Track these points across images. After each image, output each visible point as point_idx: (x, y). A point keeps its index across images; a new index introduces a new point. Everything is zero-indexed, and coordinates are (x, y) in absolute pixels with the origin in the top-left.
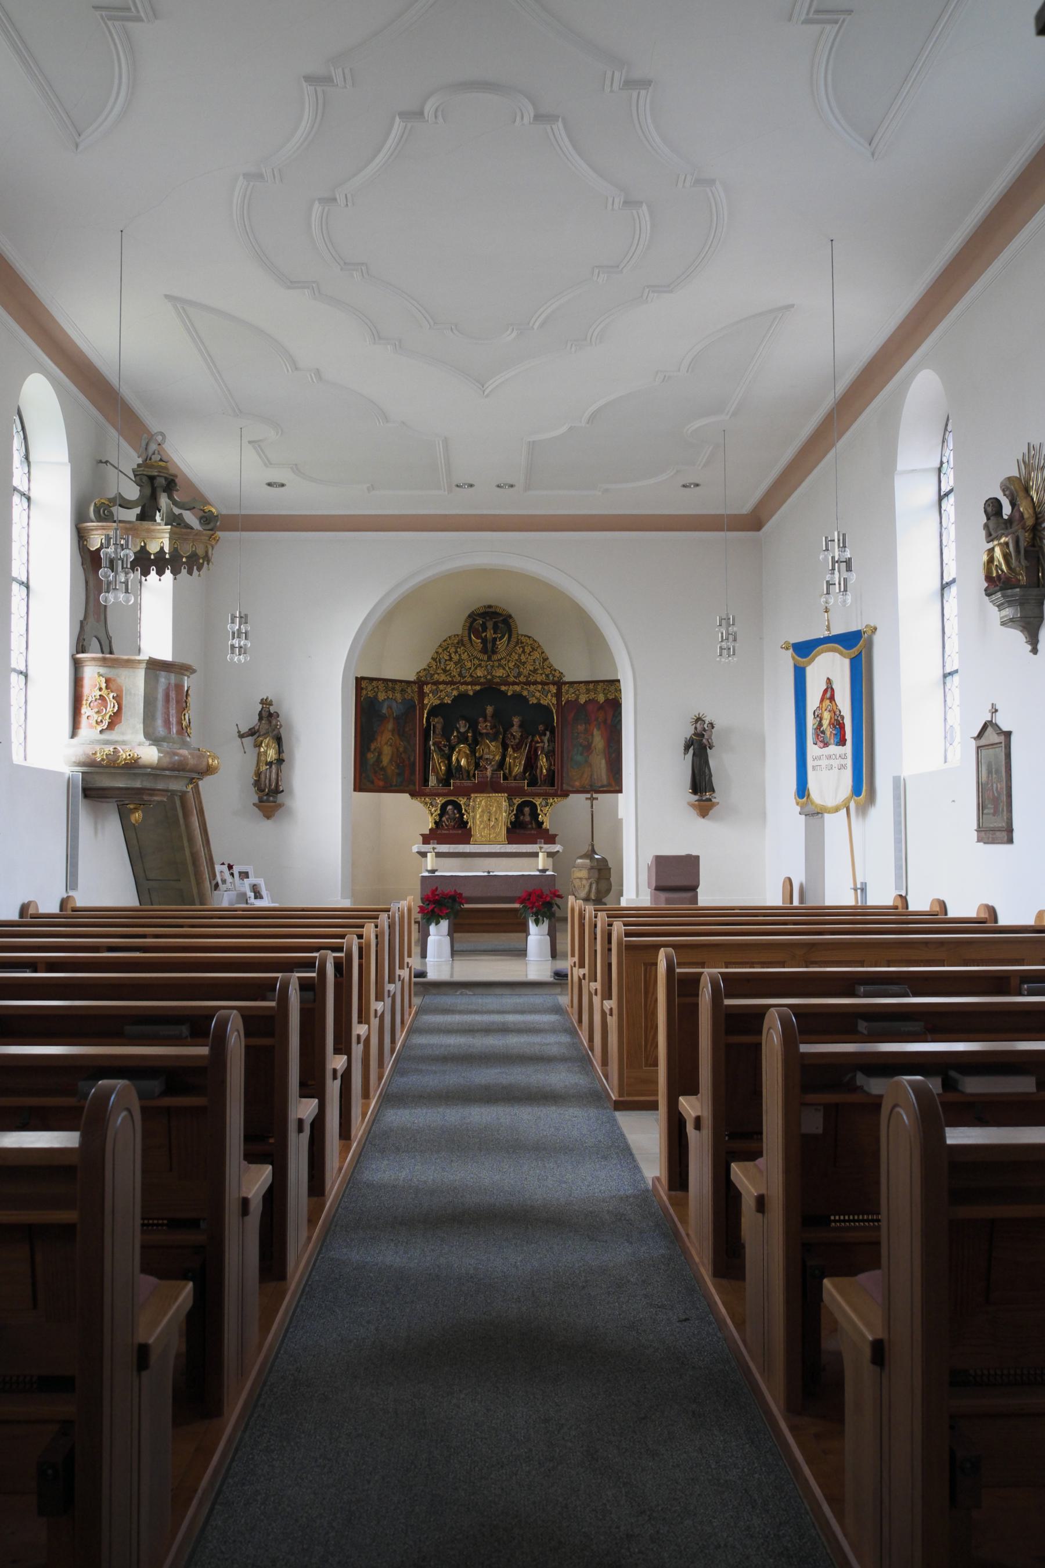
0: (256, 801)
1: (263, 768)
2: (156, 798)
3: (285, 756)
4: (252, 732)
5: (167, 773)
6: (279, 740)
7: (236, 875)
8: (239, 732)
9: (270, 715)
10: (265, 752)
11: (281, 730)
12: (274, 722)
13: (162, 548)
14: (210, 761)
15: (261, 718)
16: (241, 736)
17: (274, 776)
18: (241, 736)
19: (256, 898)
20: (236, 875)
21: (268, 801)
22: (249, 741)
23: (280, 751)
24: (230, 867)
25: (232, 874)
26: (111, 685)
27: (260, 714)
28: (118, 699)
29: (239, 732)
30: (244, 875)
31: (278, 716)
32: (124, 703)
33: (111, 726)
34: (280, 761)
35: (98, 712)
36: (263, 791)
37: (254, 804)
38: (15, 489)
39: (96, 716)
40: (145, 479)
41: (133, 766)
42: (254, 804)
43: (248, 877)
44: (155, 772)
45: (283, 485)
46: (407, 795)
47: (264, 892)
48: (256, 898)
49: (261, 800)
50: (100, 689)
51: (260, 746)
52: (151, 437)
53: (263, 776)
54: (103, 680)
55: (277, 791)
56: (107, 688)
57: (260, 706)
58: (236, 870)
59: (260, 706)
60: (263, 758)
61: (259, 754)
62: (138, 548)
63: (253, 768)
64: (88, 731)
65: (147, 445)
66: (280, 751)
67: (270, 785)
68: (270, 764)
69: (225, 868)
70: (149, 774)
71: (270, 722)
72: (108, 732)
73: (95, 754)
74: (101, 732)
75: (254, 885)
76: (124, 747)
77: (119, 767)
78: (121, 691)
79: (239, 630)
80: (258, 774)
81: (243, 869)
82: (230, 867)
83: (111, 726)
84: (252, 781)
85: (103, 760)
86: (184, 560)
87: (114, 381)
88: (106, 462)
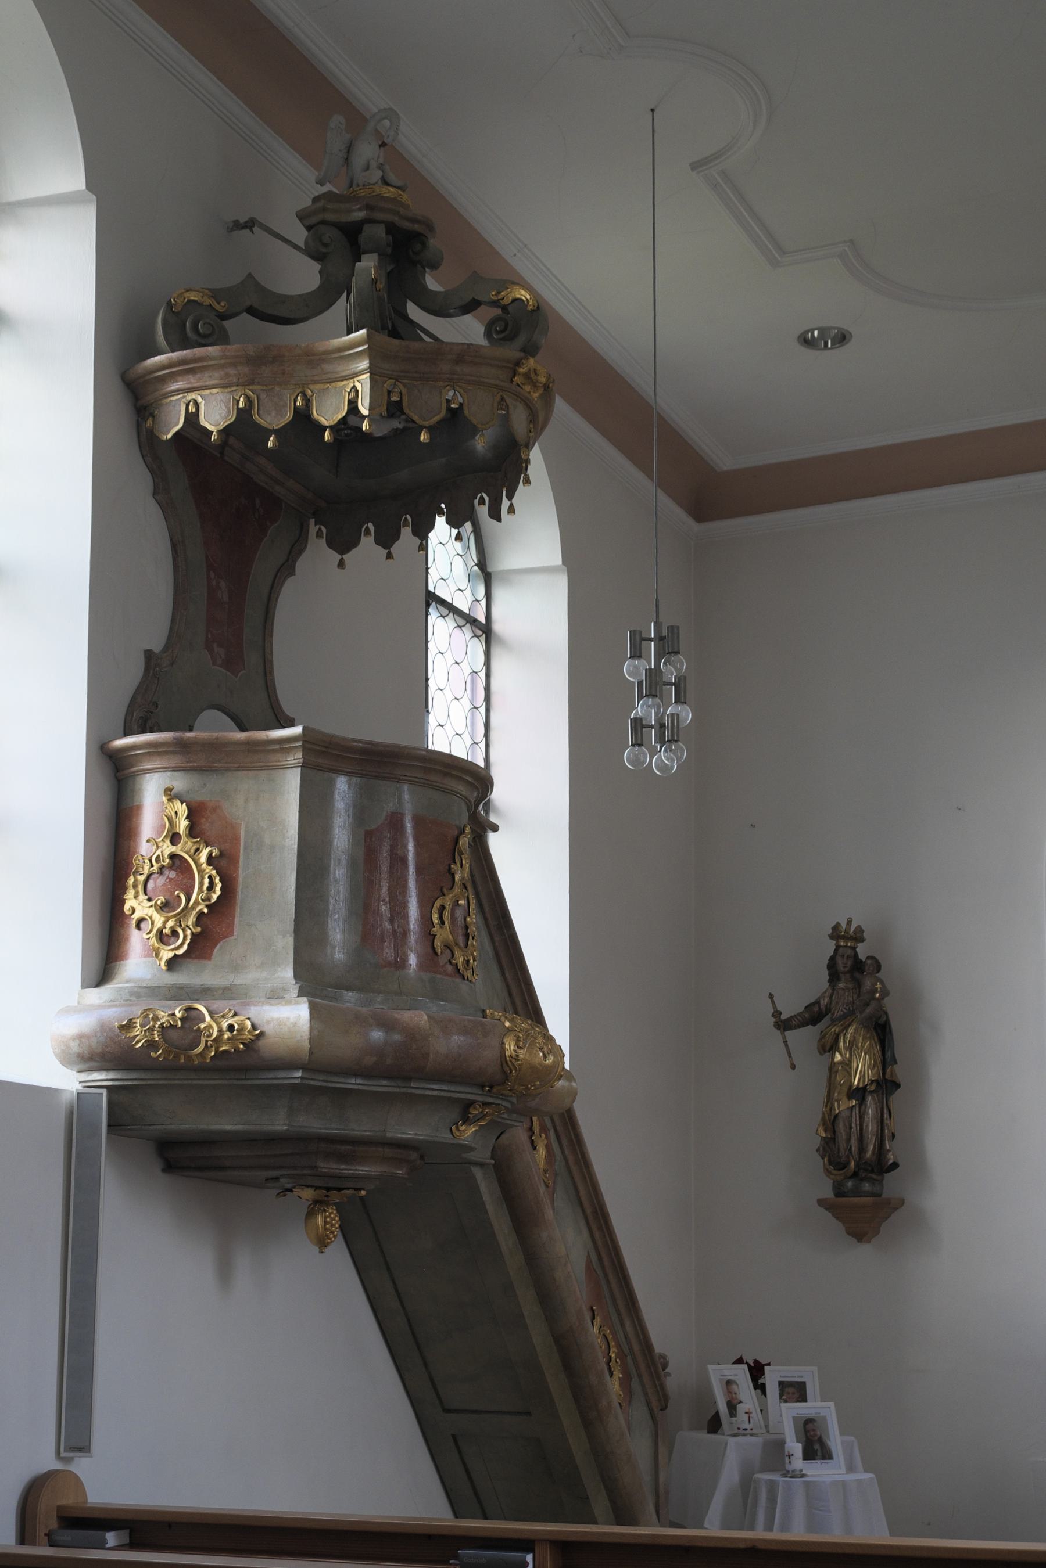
0: (828, 1193)
1: (843, 1105)
2: (364, 1169)
3: (900, 1072)
4: (813, 1015)
5: (353, 1083)
6: (881, 1031)
7: (772, 1389)
8: (777, 1014)
9: (858, 966)
10: (847, 1064)
11: (889, 1003)
12: (867, 983)
13: (353, 405)
14: (510, 1046)
15: (834, 975)
16: (783, 1025)
17: (871, 1126)
18: (783, 1025)
19: (809, 1454)
20: (772, 1389)
21: (857, 1193)
22: (805, 1037)
23: (886, 1058)
24: (757, 1371)
25: (761, 1388)
26: (205, 825)
27: (832, 965)
28: (224, 864)
29: (777, 1014)
30: (794, 1391)
31: (878, 967)
32: (242, 874)
33: (201, 946)
34: (886, 1085)
35: (165, 907)
36: (844, 1166)
37: (821, 1202)
38: (431, 598)
39: (159, 920)
40: (329, 234)
41: (245, 1062)
42: (821, 1202)
43: (803, 1398)
44: (316, 1075)
45: (842, 338)
46: (493, 840)
47: (835, 1441)
48: (809, 1454)
49: (839, 1192)
50: (175, 838)
51: (833, 1048)
52: (357, 120)
53: (841, 1126)
54: (182, 809)
55: (881, 1166)
56: (193, 831)
57: (832, 944)
58: (771, 1378)
59: (832, 944)
60: (840, 1079)
61: (832, 1068)
62: (289, 416)
63: (818, 1109)
64: (140, 963)
65: (349, 149)
66: (886, 1058)
67: (862, 1149)
68: (859, 1094)
69: (742, 1375)
70: (296, 1090)
71: (859, 984)
72: (192, 965)
73: (129, 1026)
74: (172, 964)
75: (809, 1421)
76: (217, 1005)
77: (202, 1069)
78: (236, 839)
79: (654, 675)
80: (830, 1122)
81: (792, 1373)
82: (757, 1371)
83: (201, 946)
84: (817, 1142)
85: (151, 1045)
86: (423, 437)
87: (642, 381)
88: (250, 225)
